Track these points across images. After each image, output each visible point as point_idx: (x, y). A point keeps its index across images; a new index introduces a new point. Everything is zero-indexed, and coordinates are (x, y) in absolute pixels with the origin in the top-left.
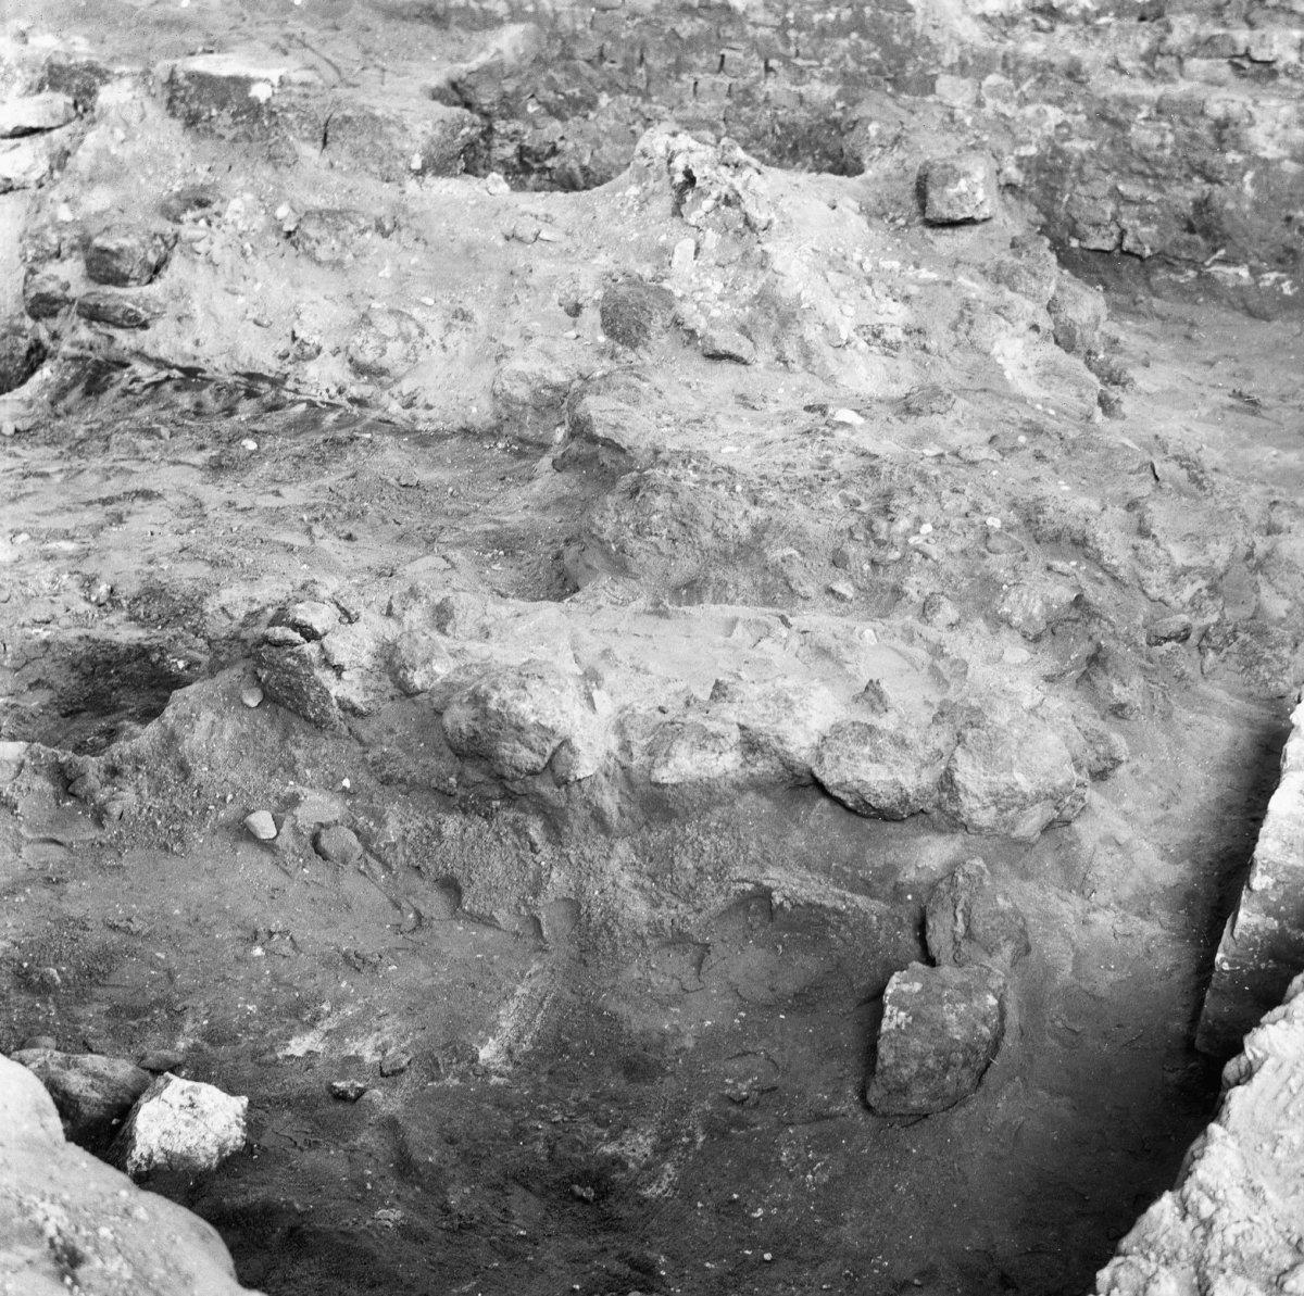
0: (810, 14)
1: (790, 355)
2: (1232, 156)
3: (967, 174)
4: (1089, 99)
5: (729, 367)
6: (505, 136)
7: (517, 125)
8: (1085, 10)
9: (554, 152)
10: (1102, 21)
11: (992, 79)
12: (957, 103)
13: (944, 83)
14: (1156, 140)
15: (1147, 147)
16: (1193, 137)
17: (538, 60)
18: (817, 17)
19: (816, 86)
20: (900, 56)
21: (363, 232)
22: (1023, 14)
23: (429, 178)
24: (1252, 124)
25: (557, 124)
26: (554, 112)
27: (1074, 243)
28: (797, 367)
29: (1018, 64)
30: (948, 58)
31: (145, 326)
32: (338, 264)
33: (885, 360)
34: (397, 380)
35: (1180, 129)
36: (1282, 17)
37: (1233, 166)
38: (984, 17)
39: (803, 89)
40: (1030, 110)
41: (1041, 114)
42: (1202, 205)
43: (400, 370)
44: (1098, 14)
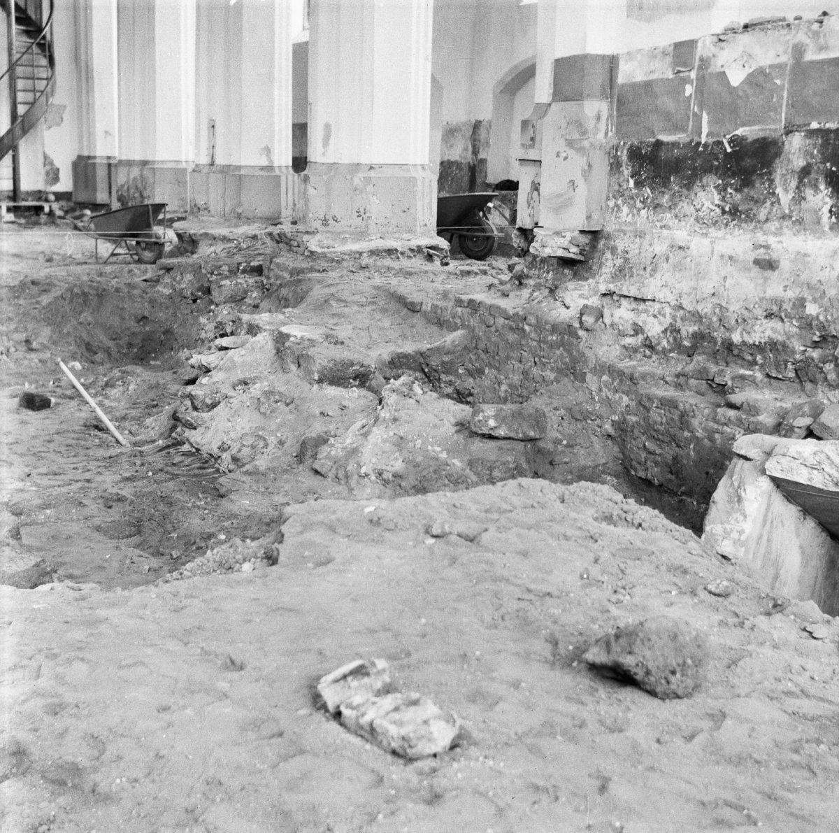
0: (547, 336)
1: (340, 476)
2: (686, 434)
3: (482, 411)
4: (636, 392)
5: (319, 477)
6: (446, 382)
7: (451, 378)
8: (664, 348)
9: (471, 394)
10: (672, 355)
11: (605, 378)
12: (593, 389)
13: (589, 377)
14: (659, 419)
15: (656, 423)
16: (672, 419)
17: (465, 348)
18: (550, 338)
19: (548, 373)
20: (575, 361)
21: (277, 402)
22: (640, 347)
23: (325, 385)
24: (694, 417)
25: (471, 380)
26: (470, 373)
27: (633, 473)
28: (342, 482)
29: (614, 371)
30: (591, 365)
31: (195, 428)
32: (265, 414)
33: (382, 487)
34: (244, 465)
35: (668, 414)
36: (739, 362)
37: (686, 439)
38: (624, 346)
39: (544, 374)
40: (617, 396)
41: (621, 398)
42: (676, 459)
43: (245, 461)
44: (670, 351)
